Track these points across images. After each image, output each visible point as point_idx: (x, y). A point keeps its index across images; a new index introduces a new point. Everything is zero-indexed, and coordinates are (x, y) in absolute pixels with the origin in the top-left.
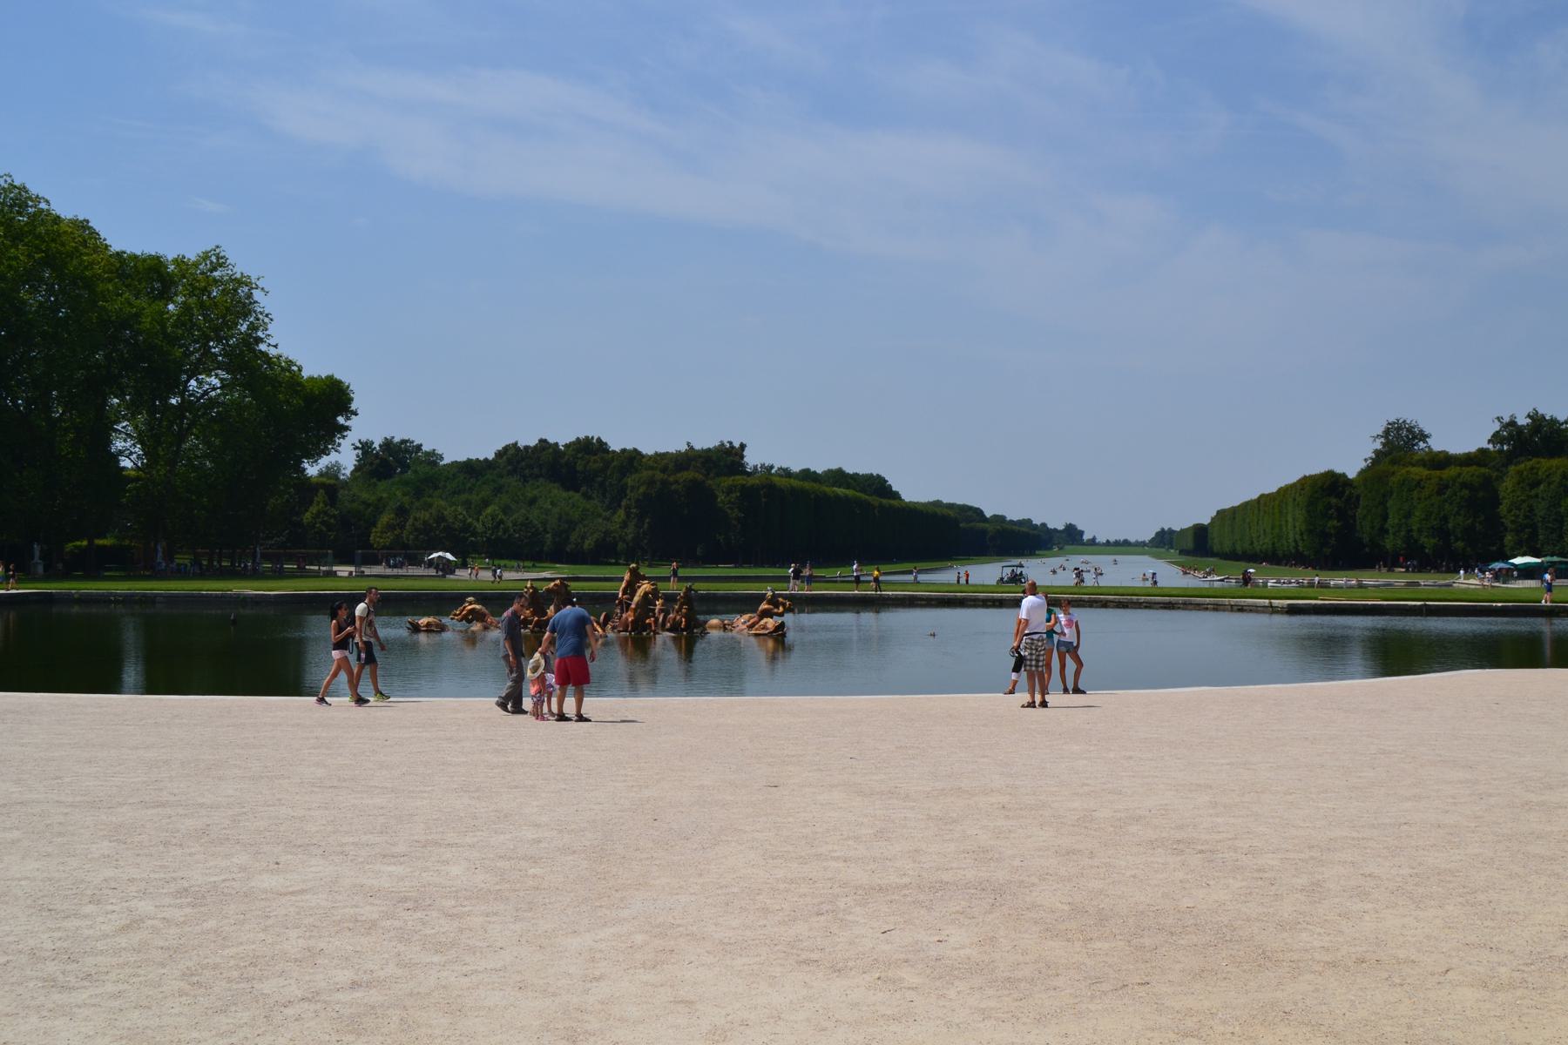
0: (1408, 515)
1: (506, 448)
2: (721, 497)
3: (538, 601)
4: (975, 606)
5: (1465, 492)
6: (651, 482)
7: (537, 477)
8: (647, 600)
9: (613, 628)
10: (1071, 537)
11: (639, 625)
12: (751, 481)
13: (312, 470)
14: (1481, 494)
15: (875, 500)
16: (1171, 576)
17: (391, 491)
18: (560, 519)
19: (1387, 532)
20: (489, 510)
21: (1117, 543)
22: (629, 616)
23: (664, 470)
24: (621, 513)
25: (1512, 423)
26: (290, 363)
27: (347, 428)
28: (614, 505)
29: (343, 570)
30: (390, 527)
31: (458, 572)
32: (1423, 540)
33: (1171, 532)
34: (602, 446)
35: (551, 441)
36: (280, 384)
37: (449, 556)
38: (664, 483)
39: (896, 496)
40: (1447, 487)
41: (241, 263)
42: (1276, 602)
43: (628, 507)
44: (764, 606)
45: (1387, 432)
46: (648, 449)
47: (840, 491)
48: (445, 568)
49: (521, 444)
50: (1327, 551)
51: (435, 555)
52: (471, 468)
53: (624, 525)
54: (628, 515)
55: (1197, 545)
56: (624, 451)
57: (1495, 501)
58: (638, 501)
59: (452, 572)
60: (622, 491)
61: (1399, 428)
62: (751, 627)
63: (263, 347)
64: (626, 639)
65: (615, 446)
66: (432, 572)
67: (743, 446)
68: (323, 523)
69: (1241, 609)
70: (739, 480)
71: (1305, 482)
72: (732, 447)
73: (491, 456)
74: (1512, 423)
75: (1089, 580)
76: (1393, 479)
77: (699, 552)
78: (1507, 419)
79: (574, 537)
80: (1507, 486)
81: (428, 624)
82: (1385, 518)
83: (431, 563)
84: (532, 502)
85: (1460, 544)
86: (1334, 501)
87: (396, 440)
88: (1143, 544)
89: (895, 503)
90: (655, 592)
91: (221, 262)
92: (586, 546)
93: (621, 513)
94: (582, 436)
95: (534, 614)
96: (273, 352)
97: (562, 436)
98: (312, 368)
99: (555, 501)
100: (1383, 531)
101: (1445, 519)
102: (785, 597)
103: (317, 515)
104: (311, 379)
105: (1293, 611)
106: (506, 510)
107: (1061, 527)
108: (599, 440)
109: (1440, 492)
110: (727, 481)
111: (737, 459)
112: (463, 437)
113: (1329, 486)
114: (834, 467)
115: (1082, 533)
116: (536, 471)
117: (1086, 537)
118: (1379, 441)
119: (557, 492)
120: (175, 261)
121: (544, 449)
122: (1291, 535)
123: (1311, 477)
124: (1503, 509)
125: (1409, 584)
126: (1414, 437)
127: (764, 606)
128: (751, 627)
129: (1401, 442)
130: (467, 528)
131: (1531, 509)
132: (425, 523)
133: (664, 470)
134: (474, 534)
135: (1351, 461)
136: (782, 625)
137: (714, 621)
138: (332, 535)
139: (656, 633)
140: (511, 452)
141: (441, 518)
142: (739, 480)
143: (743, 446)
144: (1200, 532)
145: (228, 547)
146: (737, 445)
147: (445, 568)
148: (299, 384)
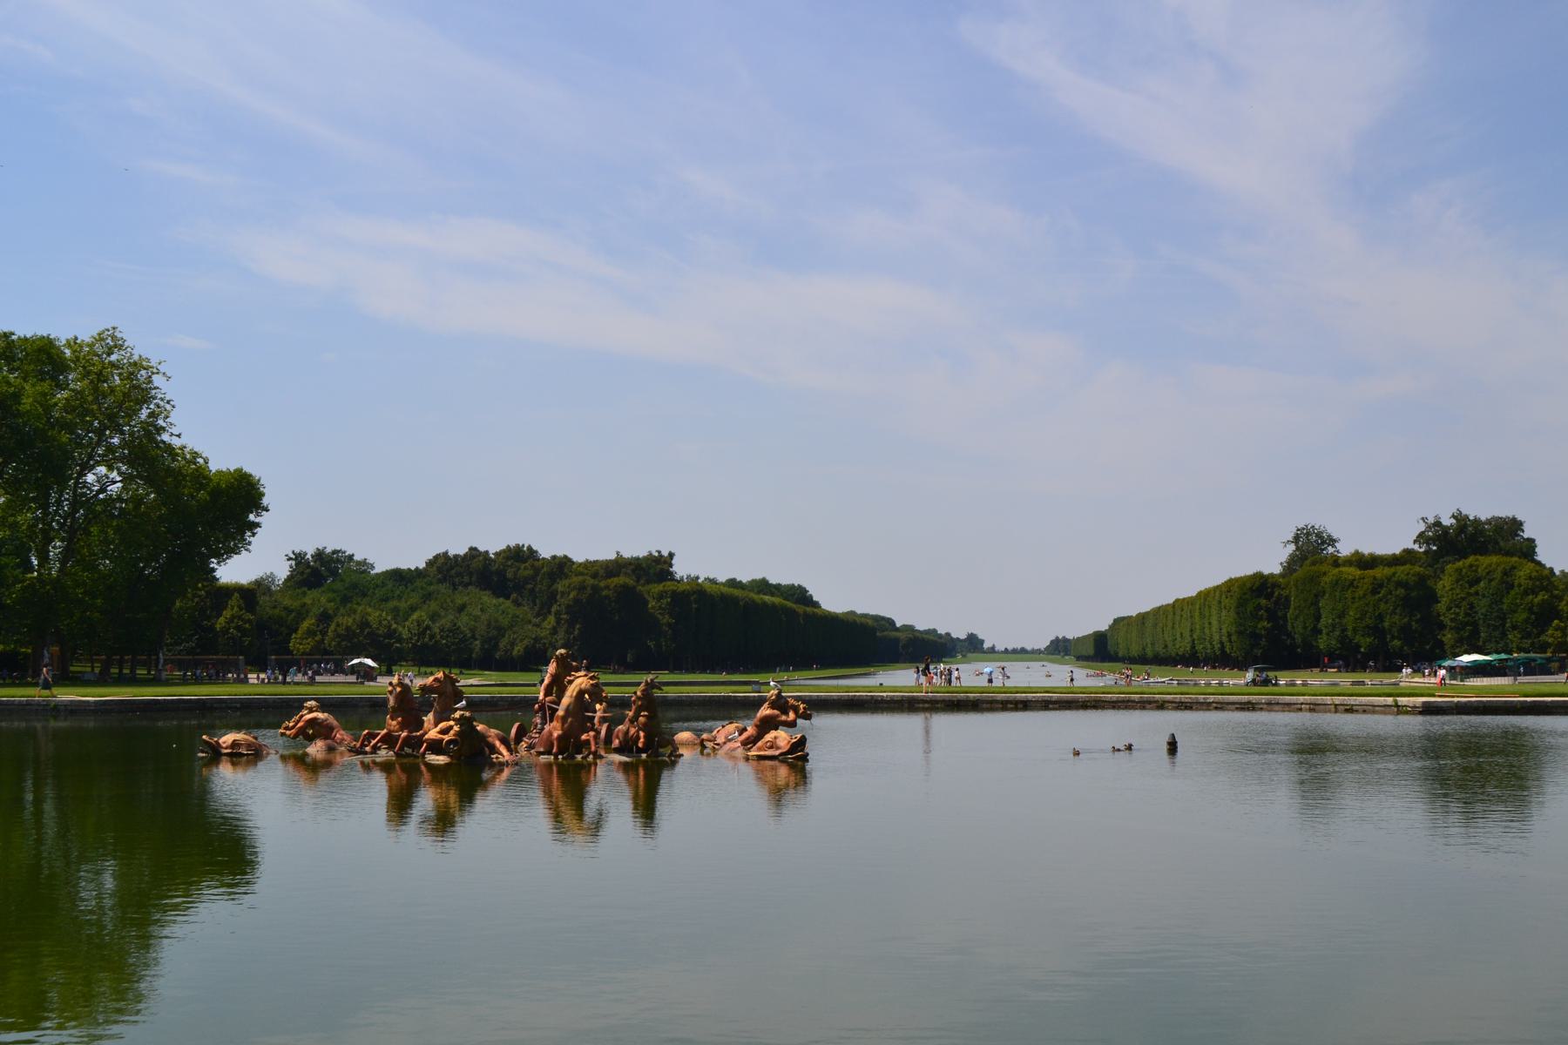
0: (1342, 615)
1: (437, 557)
2: (652, 603)
3: (410, 708)
4: (1060, 708)
5: (1401, 591)
6: (582, 588)
7: (466, 585)
8: (582, 705)
9: (530, 747)
10: (973, 645)
11: (569, 743)
12: (681, 588)
13: (233, 571)
14: (1414, 594)
15: (800, 609)
16: (1085, 679)
17: (318, 599)
18: (489, 625)
19: (1320, 632)
20: (415, 616)
21: (1015, 651)
22: (555, 729)
23: (595, 576)
24: (552, 619)
26: (195, 455)
27: (258, 525)
28: (543, 612)
29: (252, 677)
30: (310, 633)
31: (380, 679)
32: (1358, 639)
33: (1065, 640)
34: (532, 552)
35: (482, 549)
36: (184, 477)
37: (369, 662)
38: (594, 588)
39: (816, 605)
40: (1381, 586)
41: (140, 344)
42: (1403, 700)
43: (558, 614)
44: (765, 711)
45: (1296, 539)
46: (578, 557)
47: (767, 598)
48: (367, 674)
50: (1258, 652)
51: (355, 661)
52: (398, 576)
53: (554, 631)
54: (558, 621)
55: (1099, 649)
56: (554, 557)
57: (1433, 598)
58: (568, 606)
59: (374, 679)
60: (553, 597)
61: (1308, 534)
62: (750, 742)
63: (165, 437)
64: (549, 766)
65: (545, 552)
66: (352, 678)
67: (671, 555)
68: (238, 628)
69: (1350, 710)
72: (661, 556)
73: (422, 565)
74: (1438, 524)
75: (998, 683)
76: (1326, 579)
77: (629, 658)
78: (1431, 520)
79: (503, 643)
80: (1445, 585)
81: (235, 744)
82: (1318, 618)
83: (353, 670)
84: (462, 608)
85: (1397, 643)
86: (1263, 602)
87: (329, 550)
88: (1039, 652)
90: (596, 692)
91: (118, 345)
92: (515, 652)
93: (552, 619)
94: (512, 544)
95: (402, 727)
96: (176, 442)
97: (493, 544)
98: (220, 460)
99: (485, 607)
100: (1316, 631)
101: (1380, 618)
102: (797, 699)
103: (231, 620)
104: (219, 472)
105: (1428, 710)
106: (434, 617)
107: (963, 636)
108: (530, 548)
109: (1374, 592)
110: (657, 588)
112: (394, 544)
113: (1259, 586)
114: (758, 577)
115: (982, 642)
116: (466, 579)
117: (986, 646)
118: (1292, 547)
119: (488, 599)
120: (68, 344)
121: (474, 557)
122: (1216, 637)
123: (1237, 580)
124: (1441, 607)
125: (1354, 683)
127: (765, 711)
129: (1311, 547)
130: (391, 634)
131: (1472, 606)
132: (348, 628)
133: (595, 576)
134: (400, 640)
135: (1271, 559)
136: (802, 742)
137: (684, 736)
138: (247, 641)
139: (597, 756)
140: (441, 561)
141: (364, 624)
143: (671, 555)
144: (1100, 639)
145: (127, 651)
146: (665, 554)
147: (367, 674)
148: (205, 477)
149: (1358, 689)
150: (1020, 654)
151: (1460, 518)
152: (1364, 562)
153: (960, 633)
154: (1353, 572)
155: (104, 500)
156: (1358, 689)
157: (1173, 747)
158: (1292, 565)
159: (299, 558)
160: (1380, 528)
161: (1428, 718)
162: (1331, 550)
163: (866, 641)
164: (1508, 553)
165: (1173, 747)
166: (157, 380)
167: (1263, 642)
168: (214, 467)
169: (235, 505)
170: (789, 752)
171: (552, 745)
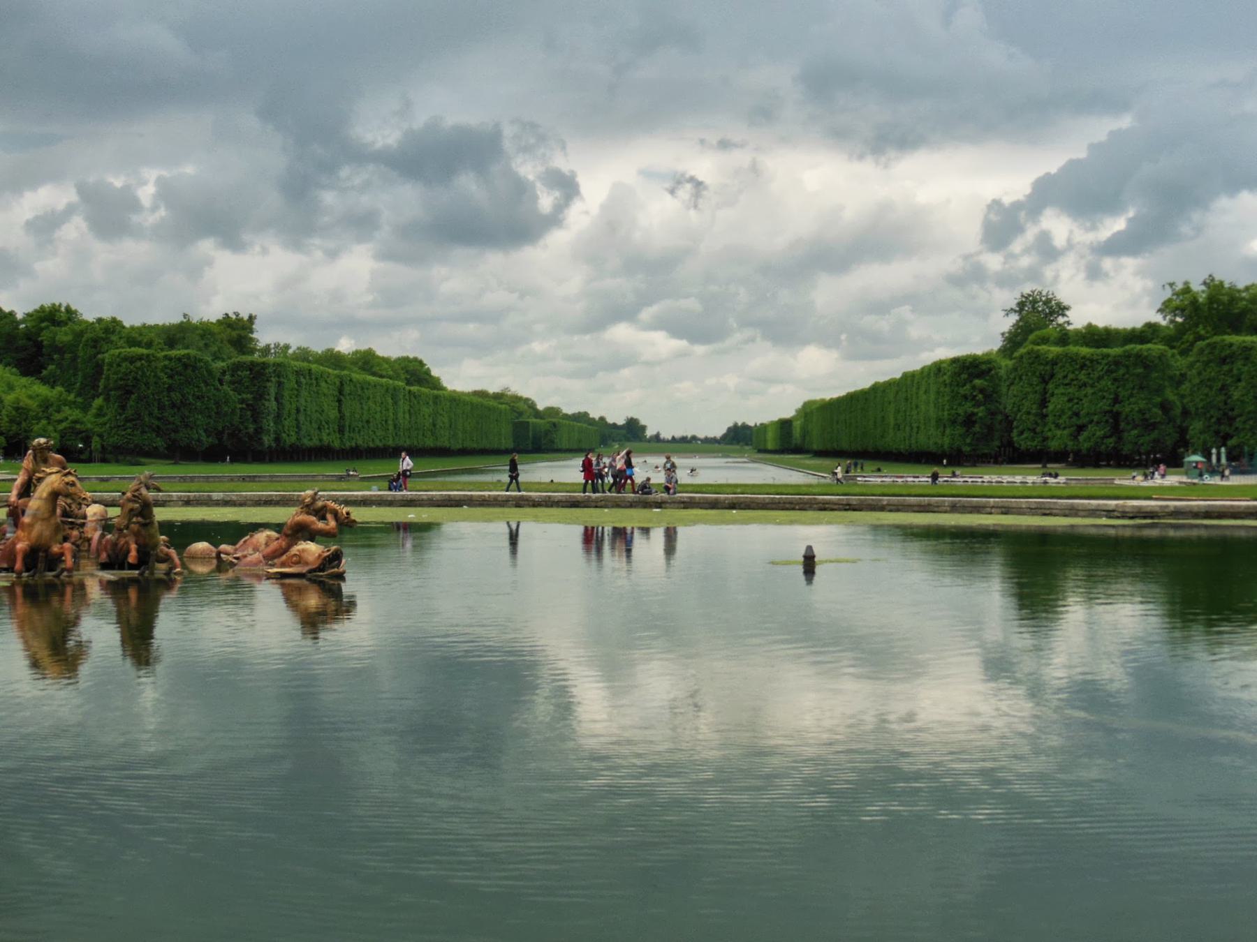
21: (684, 440)
25: (1187, 290)
33: (745, 427)
39: (435, 384)
45: (1021, 305)
52: (386, 360)
55: (784, 440)
56: (100, 320)
67: (251, 319)
74: (1187, 290)
78: (1179, 286)
82: (1043, 403)
89: (440, 392)
107: (621, 422)
108: (68, 309)
111: (243, 333)
113: (969, 369)
115: (644, 428)
117: (649, 433)
118: (1014, 318)
126: (1051, 313)
128: (270, 558)
142: (247, 358)
146: (246, 318)
150: (687, 444)
151: (1215, 288)
152: (1097, 337)
157: (809, 564)
158: (1014, 340)
161: (303, 290)
162: (1061, 320)
163: (516, 433)
165: (809, 564)
167: (977, 428)
170: (321, 568)
171: (14, 561)
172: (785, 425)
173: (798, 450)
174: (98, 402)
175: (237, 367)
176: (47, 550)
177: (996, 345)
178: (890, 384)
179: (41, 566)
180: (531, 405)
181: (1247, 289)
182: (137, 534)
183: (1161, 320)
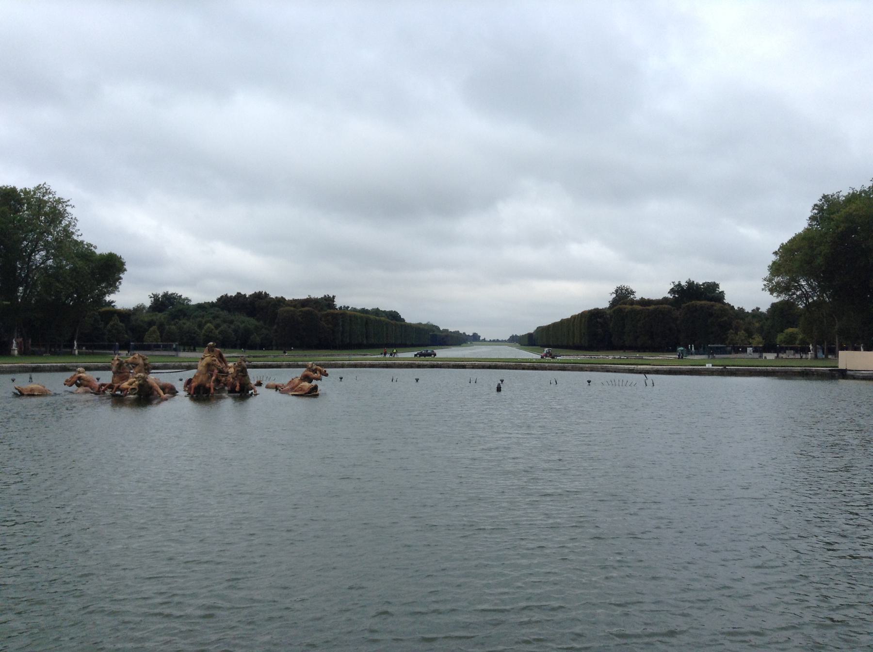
10: (475, 338)
12: (336, 312)
17: (160, 316)
21: (494, 341)
23: (295, 306)
25: (679, 285)
34: (266, 295)
35: (243, 293)
39: (403, 320)
45: (617, 291)
46: (288, 297)
49: (229, 295)
52: (201, 307)
55: (529, 341)
63: (75, 237)
65: (273, 295)
67: (334, 297)
70: (332, 311)
71: (583, 315)
74: (679, 285)
78: (677, 283)
94: (257, 291)
96: (79, 239)
98: (102, 248)
99: (244, 321)
106: (217, 326)
118: (614, 295)
129: (622, 296)
133: (295, 306)
142: (332, 311)
143: (334, 297)
149: (640, 362)
151: (691, 284)
152: (644, 302)
153: (470, 333)
154: (639, 307)
155: (43, 268)
156: (640, 362)
158: (614, 303)
159: (155, 297)
160: (653, 284)
164: (711, 300)
166: (68, 209)
168: (98, 252)
169: (110, 269)
172: (530, 335)
173: (534, 345)
174: (275, 327)
175: (327, 315)
176: (204, 386)
177: (607, 305)
178: (567, 320)
179: (201, 392)
180: (437, 328)
181: (703, 284)
182: (240, 380)
183: (670, 296)
